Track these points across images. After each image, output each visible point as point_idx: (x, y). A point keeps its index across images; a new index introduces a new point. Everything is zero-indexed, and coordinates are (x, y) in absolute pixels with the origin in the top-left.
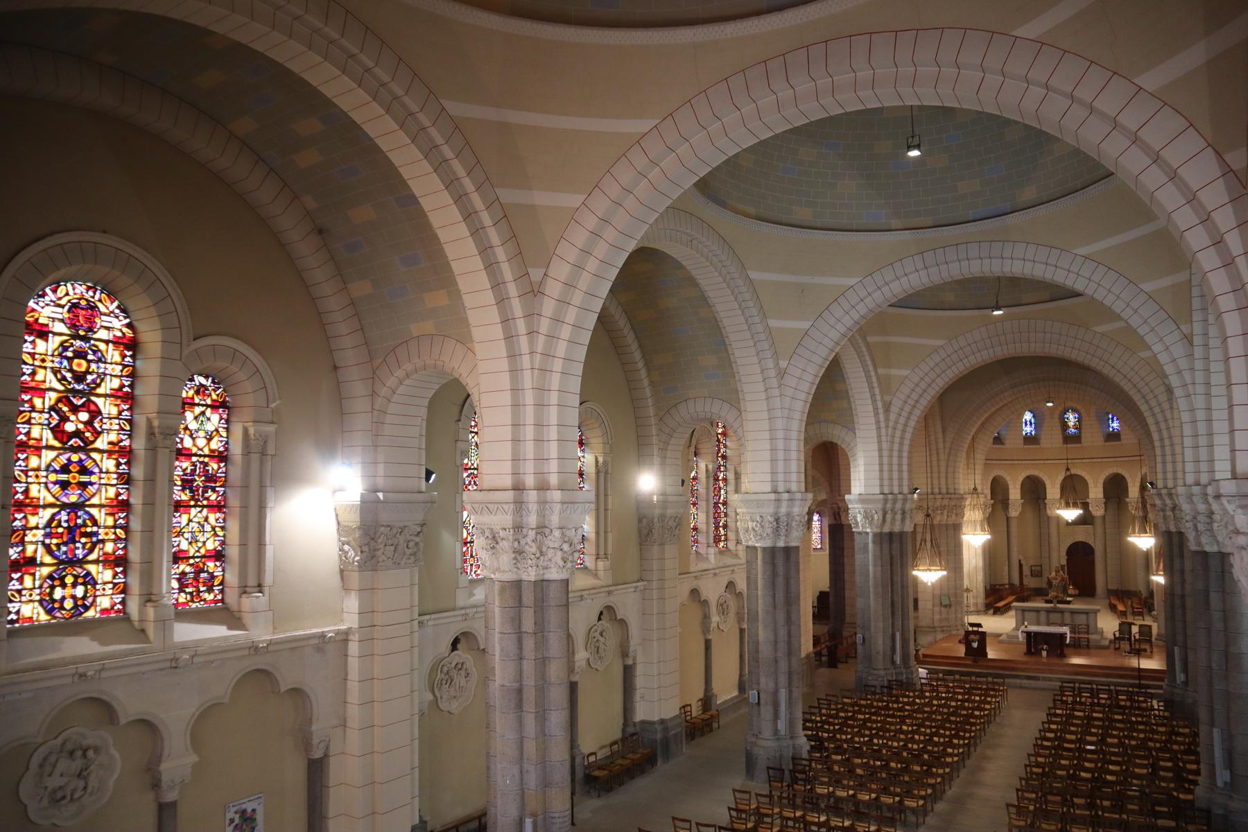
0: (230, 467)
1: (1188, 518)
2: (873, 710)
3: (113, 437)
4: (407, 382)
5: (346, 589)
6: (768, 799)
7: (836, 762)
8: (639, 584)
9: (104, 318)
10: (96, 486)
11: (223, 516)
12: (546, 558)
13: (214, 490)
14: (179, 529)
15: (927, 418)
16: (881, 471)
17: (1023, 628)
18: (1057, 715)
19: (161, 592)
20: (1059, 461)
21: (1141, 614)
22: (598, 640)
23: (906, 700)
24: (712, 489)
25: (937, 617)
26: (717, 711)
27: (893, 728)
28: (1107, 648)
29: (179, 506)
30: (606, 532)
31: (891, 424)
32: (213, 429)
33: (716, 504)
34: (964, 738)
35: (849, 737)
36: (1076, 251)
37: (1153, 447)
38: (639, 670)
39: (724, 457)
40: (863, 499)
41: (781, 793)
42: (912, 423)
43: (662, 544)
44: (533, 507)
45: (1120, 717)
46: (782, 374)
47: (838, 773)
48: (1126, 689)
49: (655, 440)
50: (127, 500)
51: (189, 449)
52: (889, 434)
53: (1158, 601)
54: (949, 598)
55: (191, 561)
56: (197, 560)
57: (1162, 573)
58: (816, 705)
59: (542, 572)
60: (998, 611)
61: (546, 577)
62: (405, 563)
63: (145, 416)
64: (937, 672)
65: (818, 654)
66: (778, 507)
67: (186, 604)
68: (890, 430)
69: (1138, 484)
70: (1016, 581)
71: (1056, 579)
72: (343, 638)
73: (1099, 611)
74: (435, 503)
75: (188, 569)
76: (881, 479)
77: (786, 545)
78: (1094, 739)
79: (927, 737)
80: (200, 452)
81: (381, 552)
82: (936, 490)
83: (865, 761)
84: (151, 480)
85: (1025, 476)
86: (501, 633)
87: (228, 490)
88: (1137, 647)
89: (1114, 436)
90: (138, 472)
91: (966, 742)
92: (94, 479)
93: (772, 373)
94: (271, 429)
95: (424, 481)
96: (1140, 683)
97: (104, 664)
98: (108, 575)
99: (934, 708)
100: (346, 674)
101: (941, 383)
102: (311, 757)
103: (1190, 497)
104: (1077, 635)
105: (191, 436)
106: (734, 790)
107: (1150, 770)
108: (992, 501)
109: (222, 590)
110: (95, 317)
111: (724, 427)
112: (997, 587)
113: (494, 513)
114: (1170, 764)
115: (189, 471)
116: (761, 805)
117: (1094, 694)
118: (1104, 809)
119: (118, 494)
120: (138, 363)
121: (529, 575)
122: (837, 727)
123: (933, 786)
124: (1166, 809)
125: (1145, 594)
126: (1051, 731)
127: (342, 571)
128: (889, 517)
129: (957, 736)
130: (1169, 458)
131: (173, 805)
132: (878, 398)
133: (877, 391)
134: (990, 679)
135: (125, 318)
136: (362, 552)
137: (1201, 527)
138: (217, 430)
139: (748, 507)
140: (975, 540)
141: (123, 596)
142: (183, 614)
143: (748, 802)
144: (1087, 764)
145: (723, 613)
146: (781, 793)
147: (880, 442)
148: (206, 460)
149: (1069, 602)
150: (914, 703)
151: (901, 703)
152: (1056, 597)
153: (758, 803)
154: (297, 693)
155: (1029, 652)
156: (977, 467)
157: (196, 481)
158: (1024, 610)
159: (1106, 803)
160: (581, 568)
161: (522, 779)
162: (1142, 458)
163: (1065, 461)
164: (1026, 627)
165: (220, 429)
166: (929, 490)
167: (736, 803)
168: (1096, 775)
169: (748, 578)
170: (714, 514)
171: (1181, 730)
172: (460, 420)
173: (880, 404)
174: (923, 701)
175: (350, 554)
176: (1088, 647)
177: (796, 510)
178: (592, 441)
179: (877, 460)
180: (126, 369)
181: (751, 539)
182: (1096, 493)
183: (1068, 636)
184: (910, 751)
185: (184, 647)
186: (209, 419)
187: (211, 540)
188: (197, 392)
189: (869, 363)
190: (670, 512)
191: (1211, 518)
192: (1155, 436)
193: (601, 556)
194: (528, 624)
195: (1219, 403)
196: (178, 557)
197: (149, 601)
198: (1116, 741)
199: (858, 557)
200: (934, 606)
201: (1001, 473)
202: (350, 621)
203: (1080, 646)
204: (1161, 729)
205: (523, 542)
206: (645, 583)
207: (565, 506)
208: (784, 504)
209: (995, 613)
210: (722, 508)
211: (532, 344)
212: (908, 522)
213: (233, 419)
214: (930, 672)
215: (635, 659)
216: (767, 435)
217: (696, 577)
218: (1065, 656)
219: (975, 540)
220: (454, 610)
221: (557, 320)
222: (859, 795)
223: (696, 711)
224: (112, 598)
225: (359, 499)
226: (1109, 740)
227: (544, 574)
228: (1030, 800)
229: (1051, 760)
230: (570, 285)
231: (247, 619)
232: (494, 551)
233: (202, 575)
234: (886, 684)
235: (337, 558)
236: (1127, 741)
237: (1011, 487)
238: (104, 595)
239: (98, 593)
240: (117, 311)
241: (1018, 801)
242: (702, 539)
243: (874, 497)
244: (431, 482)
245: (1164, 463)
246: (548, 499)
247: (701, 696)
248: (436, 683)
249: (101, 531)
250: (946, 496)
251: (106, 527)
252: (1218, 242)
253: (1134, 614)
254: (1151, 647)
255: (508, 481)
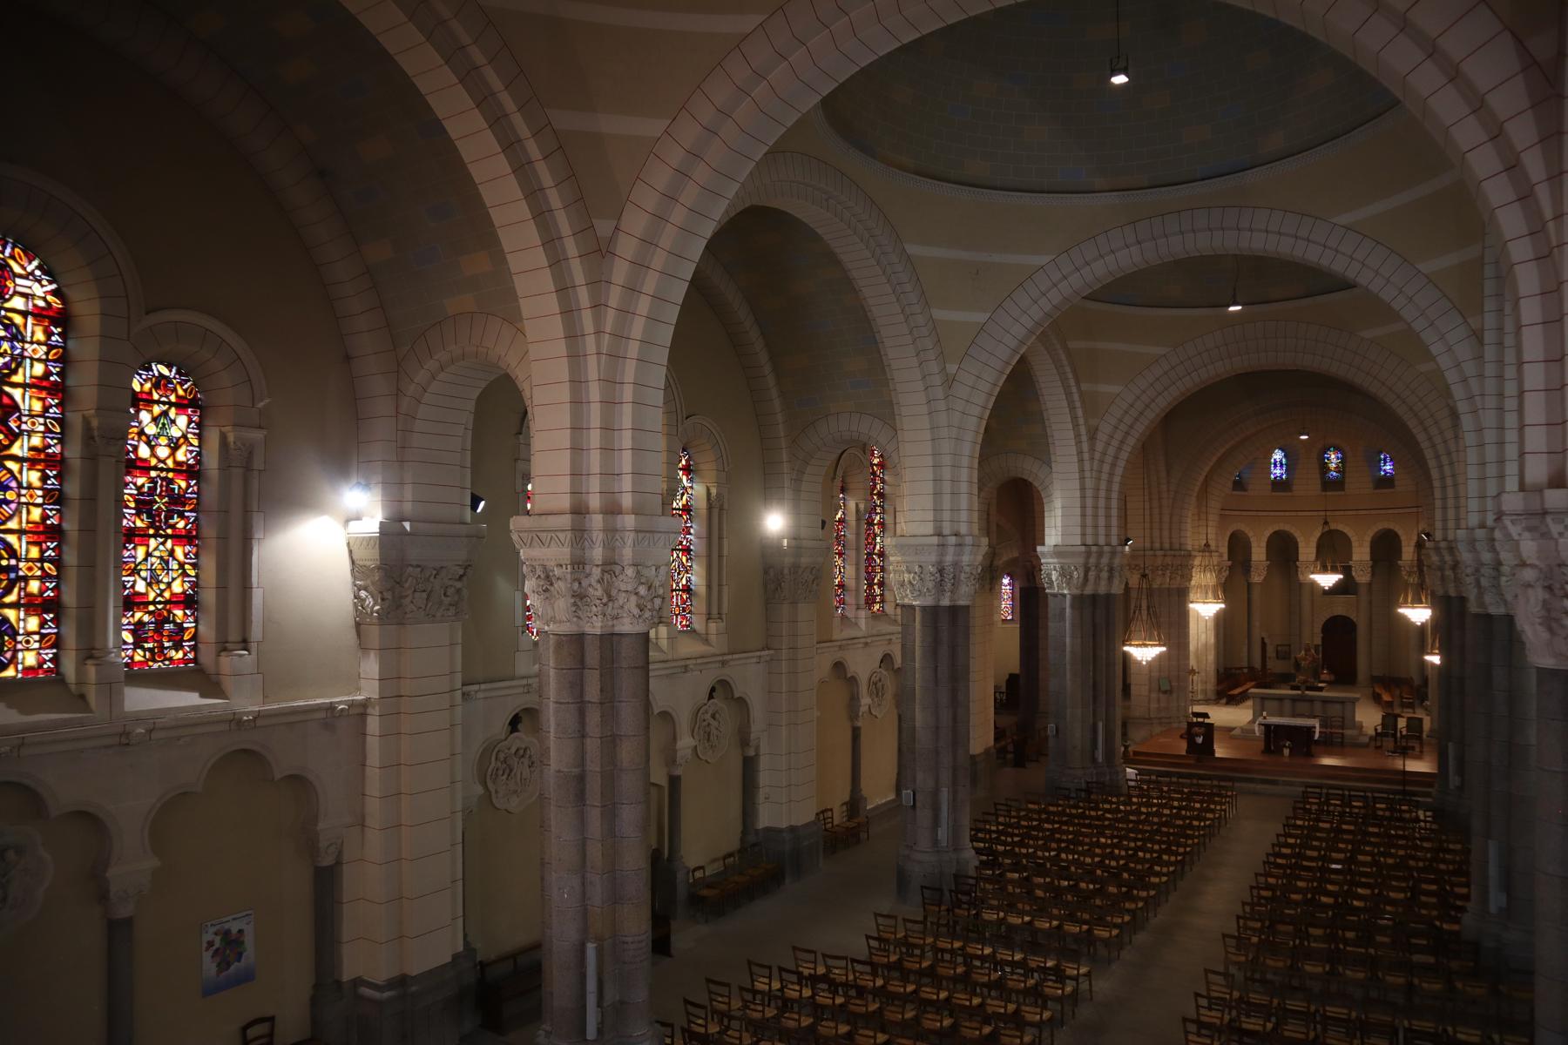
0: (203, 485)
1: (1469, 571)
2: (1065, 819)
3: (36, 441)
4: (442, 376)
5: (363, 647)
6: (921, 926)
7: (1012, 881)
8: (763, 653)
9: (18, 281)
10: (13, 506)
11: (194, 550)
12: (616, 605)
13: (181, 515)
14: (133, 565)
15: (1145, 448)
16: (1083, 515)
17: (1260, 719)
18: (1296, 827)
19: (106, 646)
20: (1315, 513)
21: (1411, 706)
22: (709, 724)
23: (1107, 806)
24: (863, 536)
25: (1154, 705)
26: (867, 817)
27: (1087, 840)
28: (1366, 746)
29: (133, 536)
30: (720, 585)
31: (1097, 456)
32: (179, 434)
33: (870, 555)
34: (1177, 854)
35: (1031, 850)
36: (1334, 220)
37: (1432, 487)
38: (764, 763)
39: (881, 495)
40: (1058, 552)
41: (939, 919)
42: (1124, 455)
43: (794, 603)
44: (598, 537)
45: (1376, 830)
46: (949, 382)
47: (1012, 894)
48: (1385, 795)
49: (786, 467)
50: (59, 525)
51: (145, 460)
52: (1095, 468)
53: (1433, 690)
54: (1170, 682)
55: (151, 608)
56: (160, 607)
57: (1437, 651)
58: (993, 811)
59: (610, 623)
60: (1233, 701)
61: (617, 629)
62: (443, 616)
63: (80, 413)
64: (1149, 773)
65: (1001, 752)
66: (942, 555)
67: (146, 663)
68: (1096, 462)
69: (1413, 543)
70: (1257, 664)
71: (1305, 659)
72: (360, 712)
73: (1357, 699)
74: (484, 538)
75: (146, 618)
76: (1083, 526)
77: (952, 604)
78: (1342, 856)
79: (1130, 852)
80: (161, 465)
81: (408, 600)
82: (1157, 545)
83: (1048, 880)
84: (90, 498)
85: (1272, 531)
86: (556, 703)
87: (201, 516)
88: (1404, 744)
89: (1387, 482)
90: (73, 489)
91: (1179, 858)
92: (10, 495)
93: (937, 380)
94: (258, 435)
95: (468, 510)
96: (1404, 790)
97: (23, 738)
98: (33, 623)
99: (1143, 817)
100: (364, 757)
101: (1163, 403)
102: (319, 865)
103: (1472, 543)
104: (1329, 730)
105: (148, 443)
106: (876, 915)
107: (1409, 894)
108: (1230, 563)
109: (195, 645)
110: (6, 280)
111: (881, 456)
112: (1233, 671)
113: (528, 545)
114: (1434, 887)
115: (146, 489)
116: (909, 933)
117: (1346, 801)
118: (1346, 942)
119: (45, 517)
120: (71, 344)
121: (594, 627)
122: (1016, 839)
123: (1132, 913)
124: (1425, 942)
125: (1417, 681)
126: (1287, 845)
127: (358, 625)
128: (1092, 574)
129: (1168, 851)
130: (1451, 502)
131: (129, 922)
132: (1081, 421)
133: (1080, 412)
134: (1215, 783)
135: (50, 282)
136: (383, 599)
137: (1484, 582)
138: (184, 436)
139: (903, 555)
140: (1205, 610)
141: (54, 651)
142: (137, 676)
143: (893, 930)
144: (1330, 887)
145: (877, 694)
146: (939, 919)
147: (1082, 478)
148: (171, 475)
149: (1321, 689)
150: (1118, 811)
151: (1101, 810)
152: (1305, 682)
153: (906, 930)
154: (298, 781)
155: (1267, 750)
156: (1210, 523)
157: (157, 502)
158: (1263, 698)
159: (1350, 935)
160: (689, 631)
161: (584, 893)
162: (1420, 510)
163: (1323, 513)
164: (1265, 718)
165: (190, 436)
166: (1148, 545)
167: (878, 930)
168: (1340, 900)
169: (903, 646)
170: (867, 567)
171: (1451, 846)
172: (520, 434)
173: (1083, 430)
174: (1128, 808)
175: (367, 602)
176: (1342, 744)
177: (966, 559)
178: (702, 467)
179: (1078, 504)
180: (54, 351)
181: (907, 595)
182: (1361, 554)
183: (1317, 730)
184: (1106, 869)
185: (138, 718)
186: (173, 422)
187: (178, 582)
188: (156, 386)
189: (1070, 376)
190: (805, 561)
191: (1498, 570)
192: (1435, 474)
193: (713, 616)
194: (593, 692)
195: (1511, 420)
196: (132, 602)
197: (91, 657)
198: (1369, 859)
199: (1052, 626)
200: (1150, 691)
201: (1242, 527)
202: (369, 690)
203: (1332, 743)
204: (1426, 845)
205: (585, 583)
206: (772, 652)
207: (641, 535)
208: (951, 550)
209: (1227, 704)
210: (878, 561)
211: (598, 320)
212: (1116, 582)
213: (206, 422)
214: (1140, 772)
215: (757, 748)
216: (929, 461)
217: (840, 646)
218: (1312, 756)
219: (1205, 610)
220: (513, 679)
221: (632, 289)
222: (1036, 923)
223: (838, 817)
224: (39, 654)
225: (378, 531)
226: (1361, 858)
227: (613, 626)
228: (1254, 929)
229: (1284, 881)
230: (648, 242)
231: (228, 683)
232: (547, 595)
233: (167, 626)
234: (1084, 786)
235: (351, 608)
236: (1382, 859)
237: (1254, 545)
238: (28, 649)
239: (19, 646)
240: (38, 273)
241: (1238, 931)
242: (849, 599)
243: (1072, 549)
244: (479, 511)
245: (1445, 508)
246: (619, 526)
247: (846, 798)
248: (490, 770)
249: (21, 565)
250: (1169, 553)
251: (28, 560)
252: (1513, 167)
253: (1403, 705)
254: (1421, 745)
255: (565, 502)
